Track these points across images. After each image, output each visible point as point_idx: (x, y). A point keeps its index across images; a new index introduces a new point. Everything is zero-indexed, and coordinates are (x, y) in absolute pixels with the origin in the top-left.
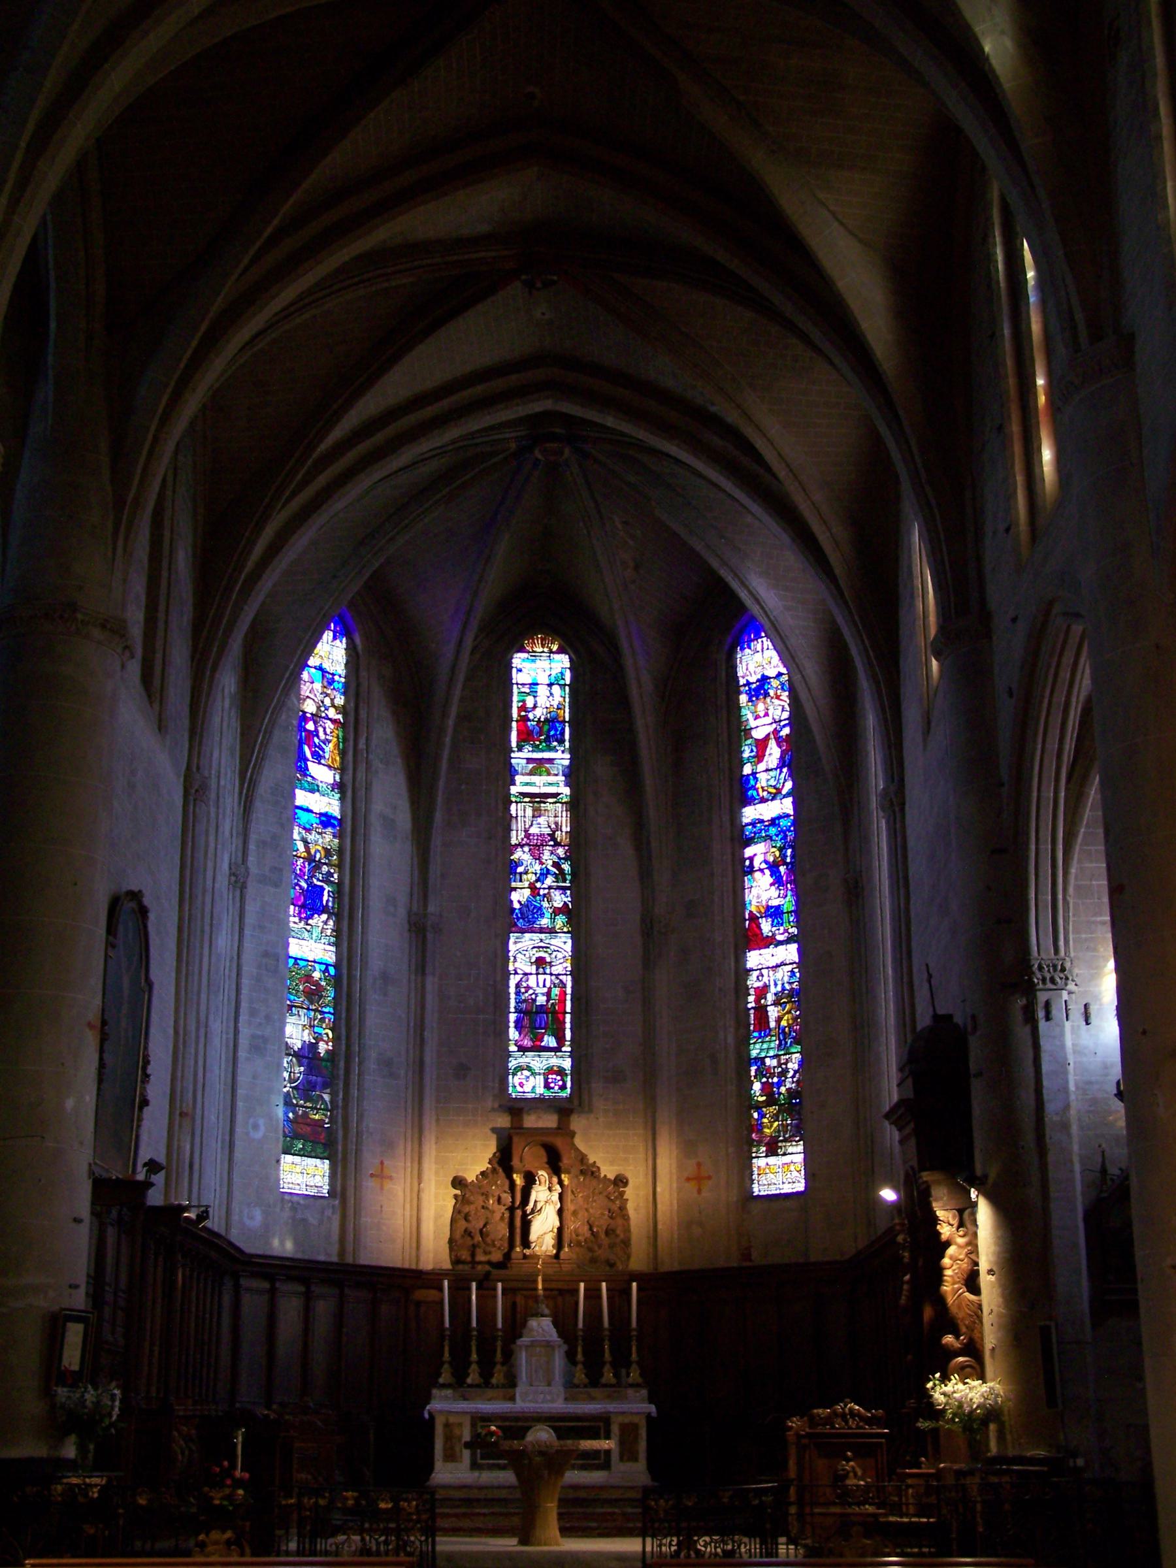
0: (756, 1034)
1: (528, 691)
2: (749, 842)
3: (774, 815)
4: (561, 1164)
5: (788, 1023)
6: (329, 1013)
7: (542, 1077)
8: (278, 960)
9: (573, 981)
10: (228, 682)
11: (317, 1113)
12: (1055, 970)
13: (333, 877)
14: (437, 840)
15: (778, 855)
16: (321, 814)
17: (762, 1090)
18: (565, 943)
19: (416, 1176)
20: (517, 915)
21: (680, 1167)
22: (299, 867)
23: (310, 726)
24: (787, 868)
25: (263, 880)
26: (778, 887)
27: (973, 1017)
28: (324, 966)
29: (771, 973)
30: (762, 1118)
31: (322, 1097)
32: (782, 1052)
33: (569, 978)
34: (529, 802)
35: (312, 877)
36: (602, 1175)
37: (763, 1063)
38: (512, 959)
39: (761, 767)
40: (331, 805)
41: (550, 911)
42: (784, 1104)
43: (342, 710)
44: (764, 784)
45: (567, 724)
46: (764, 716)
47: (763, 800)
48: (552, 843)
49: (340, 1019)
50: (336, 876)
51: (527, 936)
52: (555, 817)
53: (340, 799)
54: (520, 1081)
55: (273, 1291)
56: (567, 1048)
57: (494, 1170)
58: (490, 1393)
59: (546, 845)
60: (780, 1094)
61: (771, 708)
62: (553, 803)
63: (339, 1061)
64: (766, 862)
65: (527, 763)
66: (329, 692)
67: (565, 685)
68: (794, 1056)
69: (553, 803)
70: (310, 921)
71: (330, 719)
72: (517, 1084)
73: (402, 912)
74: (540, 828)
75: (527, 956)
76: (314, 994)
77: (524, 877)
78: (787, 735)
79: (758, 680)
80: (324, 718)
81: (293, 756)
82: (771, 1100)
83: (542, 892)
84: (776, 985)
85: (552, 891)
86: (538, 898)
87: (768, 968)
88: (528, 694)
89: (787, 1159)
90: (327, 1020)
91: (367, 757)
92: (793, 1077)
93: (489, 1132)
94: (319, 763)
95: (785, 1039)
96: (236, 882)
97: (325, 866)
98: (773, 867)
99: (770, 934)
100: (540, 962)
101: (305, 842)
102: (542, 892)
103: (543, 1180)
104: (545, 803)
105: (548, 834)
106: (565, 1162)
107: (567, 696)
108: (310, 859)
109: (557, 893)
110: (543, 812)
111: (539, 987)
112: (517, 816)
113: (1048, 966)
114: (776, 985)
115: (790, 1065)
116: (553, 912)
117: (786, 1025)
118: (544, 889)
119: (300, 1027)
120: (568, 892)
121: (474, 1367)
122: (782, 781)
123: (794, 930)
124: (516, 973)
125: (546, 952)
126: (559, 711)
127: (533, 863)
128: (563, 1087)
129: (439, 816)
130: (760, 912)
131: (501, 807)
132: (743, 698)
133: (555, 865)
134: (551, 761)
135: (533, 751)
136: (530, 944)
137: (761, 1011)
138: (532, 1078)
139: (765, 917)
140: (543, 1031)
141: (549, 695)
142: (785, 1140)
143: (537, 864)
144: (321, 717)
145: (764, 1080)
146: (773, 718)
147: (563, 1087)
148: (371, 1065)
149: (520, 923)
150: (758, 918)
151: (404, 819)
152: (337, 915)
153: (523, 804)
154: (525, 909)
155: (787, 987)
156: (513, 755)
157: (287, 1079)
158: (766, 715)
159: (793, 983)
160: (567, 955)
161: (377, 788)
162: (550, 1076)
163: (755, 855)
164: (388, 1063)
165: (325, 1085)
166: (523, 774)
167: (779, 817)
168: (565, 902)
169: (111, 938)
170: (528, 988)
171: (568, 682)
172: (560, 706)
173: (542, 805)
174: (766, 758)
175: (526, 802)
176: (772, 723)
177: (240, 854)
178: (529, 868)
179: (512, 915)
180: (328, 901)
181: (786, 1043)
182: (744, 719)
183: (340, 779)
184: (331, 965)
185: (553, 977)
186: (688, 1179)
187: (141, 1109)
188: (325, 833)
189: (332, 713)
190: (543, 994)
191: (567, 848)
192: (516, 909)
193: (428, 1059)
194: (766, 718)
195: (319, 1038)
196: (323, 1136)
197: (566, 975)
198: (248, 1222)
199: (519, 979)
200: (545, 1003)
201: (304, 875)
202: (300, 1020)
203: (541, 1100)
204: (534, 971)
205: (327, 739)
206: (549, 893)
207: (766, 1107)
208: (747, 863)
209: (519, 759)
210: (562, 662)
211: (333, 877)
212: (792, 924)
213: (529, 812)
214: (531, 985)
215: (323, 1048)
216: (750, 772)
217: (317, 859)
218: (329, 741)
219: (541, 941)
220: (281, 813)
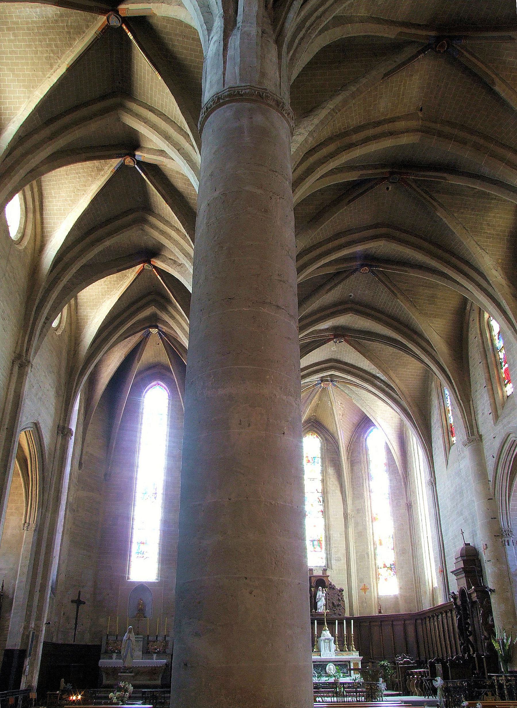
12: (509, 532)
27: (486, 545)
113: (507, 531)
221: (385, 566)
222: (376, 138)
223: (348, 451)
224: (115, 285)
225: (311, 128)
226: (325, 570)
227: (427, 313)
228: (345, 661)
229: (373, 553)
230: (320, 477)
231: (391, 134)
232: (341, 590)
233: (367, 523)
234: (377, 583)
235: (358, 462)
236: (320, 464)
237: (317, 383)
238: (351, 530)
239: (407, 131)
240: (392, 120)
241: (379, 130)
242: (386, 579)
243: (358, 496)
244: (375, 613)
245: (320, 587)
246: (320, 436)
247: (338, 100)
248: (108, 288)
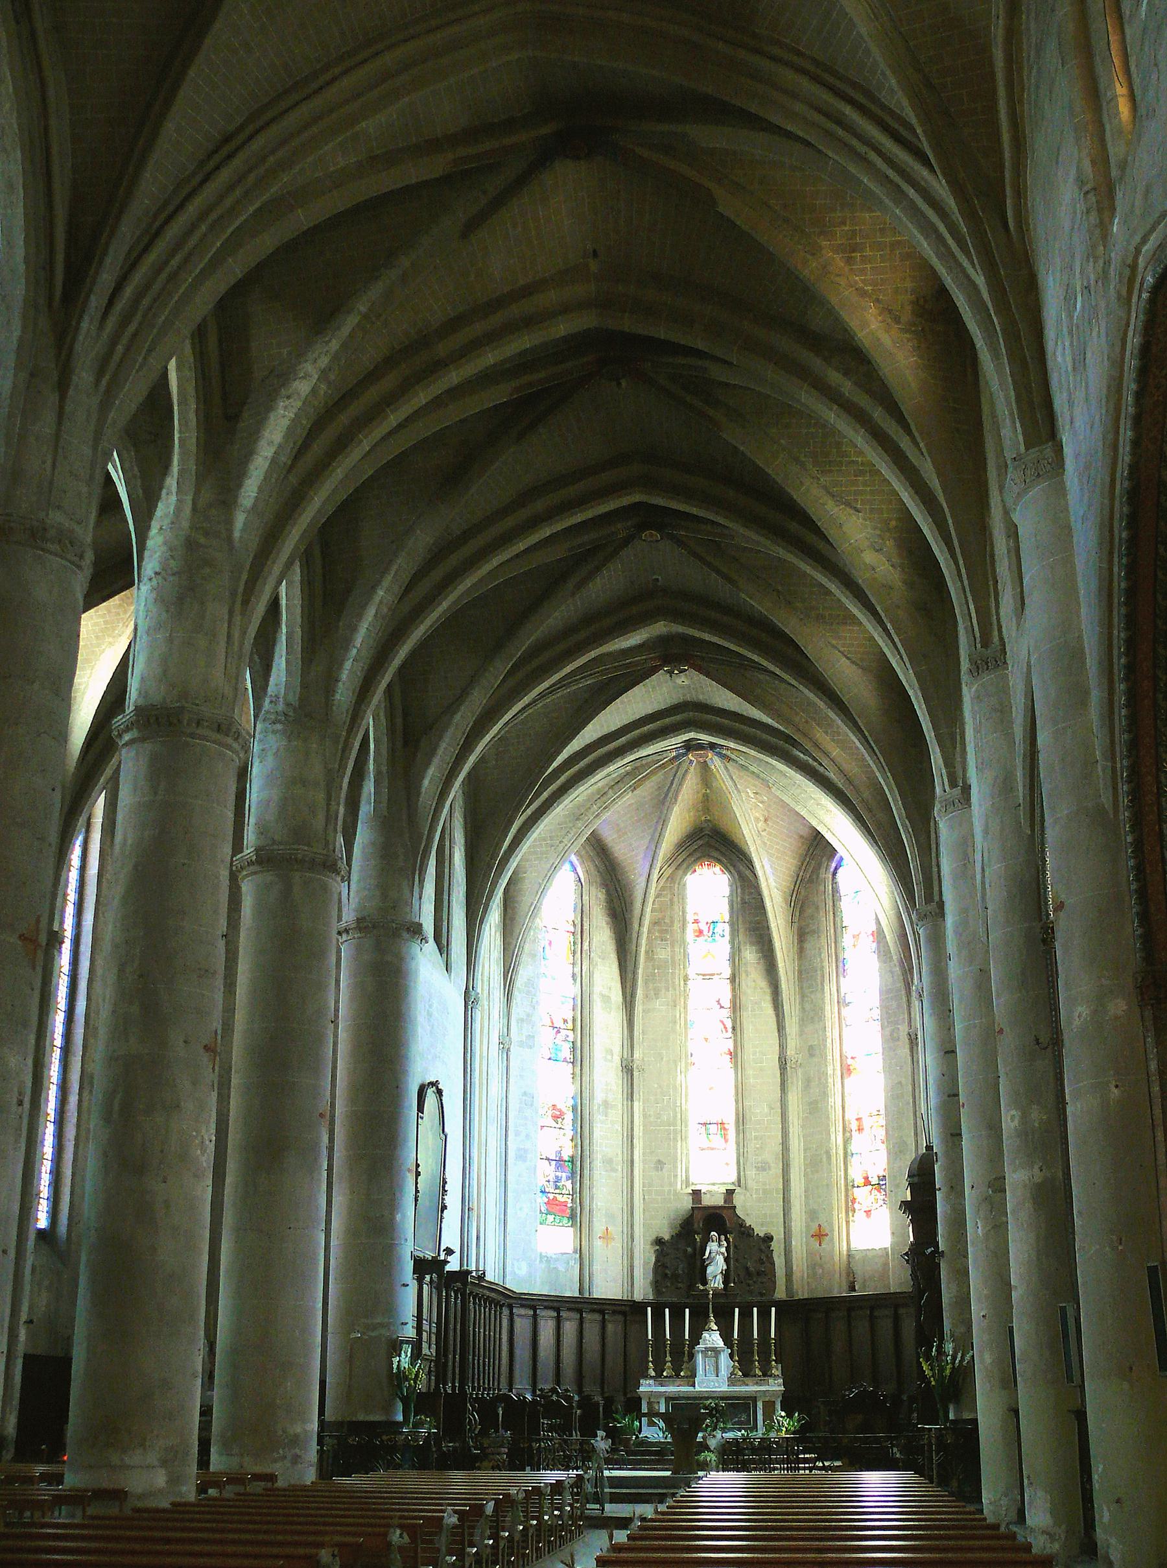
10: (494, 918)
25: (521, 1044)
55: (535, 1316)
58: (678, 1381)
103: (714, 1238)
121: (669, 1364)
148: (598, 1163)
151: (617, 995)
161: (597, 976)
164: (610, 1161)
169: (420, 1114)
177: (506, 1030)
187: (442, 1212)
193: (636, 1158)
198: (517, 1271)
221: (867, 1182)
222: (491, 338)
223: (792, 904)
224: (119, 614)
225: (324, 361)
226: (730, 1193)
227: (823, 617)
228: (745, 1398)
229: (841, 1152)
230: (727, 972)
231: (529, 322)
232: (769, 1238)
233: (830, 1080)
234: (848, 1222)
235: (814, 932)
236: (728, 937)
237: (674, 754)
238: (793, 1098)
239: (565, 309)
240: (527, 291)
241: (496, 320)
242: (868, 1212)
243: (812, 1015)
244: (839, 1290)
245: (712, 1233)
246: (727, 868)
247: (376, 291)
248: (106, 622)
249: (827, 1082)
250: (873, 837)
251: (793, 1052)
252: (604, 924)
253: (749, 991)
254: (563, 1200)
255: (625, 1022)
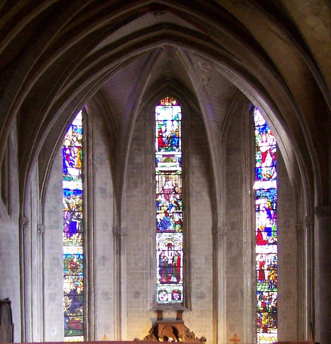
0: (259, 281)
1: (163, 124)
2: (258, 197)
3: (269, 188)
4: (178, 335)
5: (273, 279)
6: (81, 275)
7: (171, 294)
8: (59, 260)
9: (184, 253)
11: (78, 318)
13: (80, 216)
14: (124, 194)
15: (270, 205)
16: (74, 190)
17: (262, 305)
18: (180, 237)
19: (119, 332)
20: (159, 225)
21: (228, 335)
22: (66, 215)
23: (68, 152)
24: (274, 212)
25: (51, 227)
26: (270, 219)
28: (78, 256)
29: (266, 256)
30: (261, 317)
31: (79, 311)
32: (270, 291)
33: (182, 252)
34: (164, 174)
35: (71, 218)
36: (196, 337)
37: (262, 294)
38: (157, 244)
39: (264, 165)
40: (78, 185)
41: (174, 223)
42: (270, 312)
43: (82, 141)
44: (265, 173)
45: (180, 139)
46: (266, 142)
47: (264, 180)
48: (174, 193)
49: (86, 277)
50: (81, 216)
51: (164, 234)
52: (175, 181)
53: (82, 181)
54: (161, 296)
56: (181, 282)
57: (151, 336)
59: (171, 194)
60: (269, 308)
61: (268, 139)
62: (174, 175)
63: (86, 295)
64: (265, 207)
65: (163, 157)
66: (75, 134)
67: (179, 120)
68: (275, 293)
69: (174, 175)
70: (72, 238)
71: (76, 147)
72: (160, 298)
73: (110, 228)
74: (169, 186)
75: (164, 243)
76: (74, 268)
77: (162, 208)
78: (275, 152)
79: (263, 125)
80: (74, 147)
81: (62, 167)
82: (265, 310)
83: (170, 215)
84: (268, 262)
85: (174, 214)
86: (168, 217)
87: (265, 254)
88: (163, 125)
89: (271, 335)
90: (80, 278)
91: (93, 163)
92: (274, 301)
93: (149, 320)
94: (73, 167)
95: (271, 285)
96: (40, 232)
97: (77, 213)
98: (268, 211)
99: (266, 240)
100: (169, 245)
101: (68, 204)
102: (170, 215)
104: (171, 175)
105: (172, 189)
106: (180, 333)
107: (180, 126)
108: (70, 211)
109: (177, 215)
110: (170, 179)
111: (169, 257)
112: (158, 181)
114: (268, 262)
115: (273, 296)
116: (175, 223)
117: (272, 279)
118: (171, 213)
119: (69, 283)
120: (181, 214)
122: (272, 173)
123: (276, 239)
124: (159, 250)
125: (172, 241)
126: (177, 132)
127: (166, 202)
128: (180, 299)
129: (125, 186)
130: (262, 229)
131: (151, 178)
132: (257, 132)
133: (176, 202)
134: (173, 156)
135: (165, 151)
136: (165, 237)
137: (262, 271)
138: (166, 295)
139: (264, 231)
140: (171, 275)
141: (172, 125)
142: (270, 327)
143: (168, 202)
144: (72, 147)
145: (263, 301)
146: (269, 144)
147: (180, 299)
148: (99, 296)
149: (161, 229)
150: (261, 232)
151: (110, 188)
152: (83, 233)
153: (161, 175)
154: (163, 222)
155: (273, 263)
156: (156, 153)
157: (65, 306)
158: (266, 141)
159: (275, 262)
160: (181, 242)
162: (174, 294)
163: (260, 204)
165: (80, 306)
166: (161, 162)
167: (271, 189)
168: (180, 219)
170: (164, 257)
171: (180, 119)
172: (177, 130)
173: (170, 176)
174: (266, 161)
175: (162, 175)
176: (268, 146)
178: (164, 204)
179: (158, 225)
180: (78, 228)
181: (272, 287)
182: (257, 142)
183: (82, 172)
184: (81, 255)
185: (175, 252)
186: (231, 340)
188: (76, 198)
189: (77, 144)
190: (171, 259)
191: (180, 195)
192: (158, 222)
194: (266, 143)
195: (77, 286)
196: (81, 326)
197: (180, 250)
199: (160, 253)
200: (172, 263)
201: (68, 218)
202: (69, 280)
203: (170, 304)
204: (167, 249)
205: (75, 156)
206: (173, 215)
207: (263, 312)
208: (257, 207)
209: (159, 155)
210: (177, 110)
211: (80, 216)
212: (275, 236)
213: (164, 179)
214: (165, 255)
215: (79, 290)
216: (259, 167)
217: (73, 210)
218: (76, 157)
219: (170, 236)
220: (57, 197)
249: (242, 247)
250: (284, 120)
251: (221, 225)
252: (102, 142)
253: (194, 185)
254: (78, 319)
255: (115, 205)
